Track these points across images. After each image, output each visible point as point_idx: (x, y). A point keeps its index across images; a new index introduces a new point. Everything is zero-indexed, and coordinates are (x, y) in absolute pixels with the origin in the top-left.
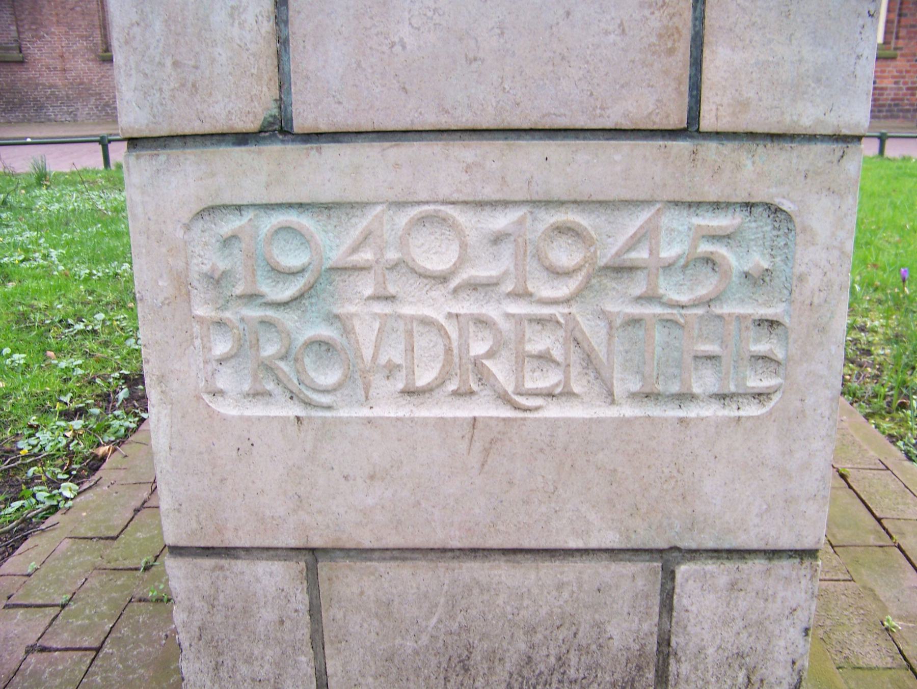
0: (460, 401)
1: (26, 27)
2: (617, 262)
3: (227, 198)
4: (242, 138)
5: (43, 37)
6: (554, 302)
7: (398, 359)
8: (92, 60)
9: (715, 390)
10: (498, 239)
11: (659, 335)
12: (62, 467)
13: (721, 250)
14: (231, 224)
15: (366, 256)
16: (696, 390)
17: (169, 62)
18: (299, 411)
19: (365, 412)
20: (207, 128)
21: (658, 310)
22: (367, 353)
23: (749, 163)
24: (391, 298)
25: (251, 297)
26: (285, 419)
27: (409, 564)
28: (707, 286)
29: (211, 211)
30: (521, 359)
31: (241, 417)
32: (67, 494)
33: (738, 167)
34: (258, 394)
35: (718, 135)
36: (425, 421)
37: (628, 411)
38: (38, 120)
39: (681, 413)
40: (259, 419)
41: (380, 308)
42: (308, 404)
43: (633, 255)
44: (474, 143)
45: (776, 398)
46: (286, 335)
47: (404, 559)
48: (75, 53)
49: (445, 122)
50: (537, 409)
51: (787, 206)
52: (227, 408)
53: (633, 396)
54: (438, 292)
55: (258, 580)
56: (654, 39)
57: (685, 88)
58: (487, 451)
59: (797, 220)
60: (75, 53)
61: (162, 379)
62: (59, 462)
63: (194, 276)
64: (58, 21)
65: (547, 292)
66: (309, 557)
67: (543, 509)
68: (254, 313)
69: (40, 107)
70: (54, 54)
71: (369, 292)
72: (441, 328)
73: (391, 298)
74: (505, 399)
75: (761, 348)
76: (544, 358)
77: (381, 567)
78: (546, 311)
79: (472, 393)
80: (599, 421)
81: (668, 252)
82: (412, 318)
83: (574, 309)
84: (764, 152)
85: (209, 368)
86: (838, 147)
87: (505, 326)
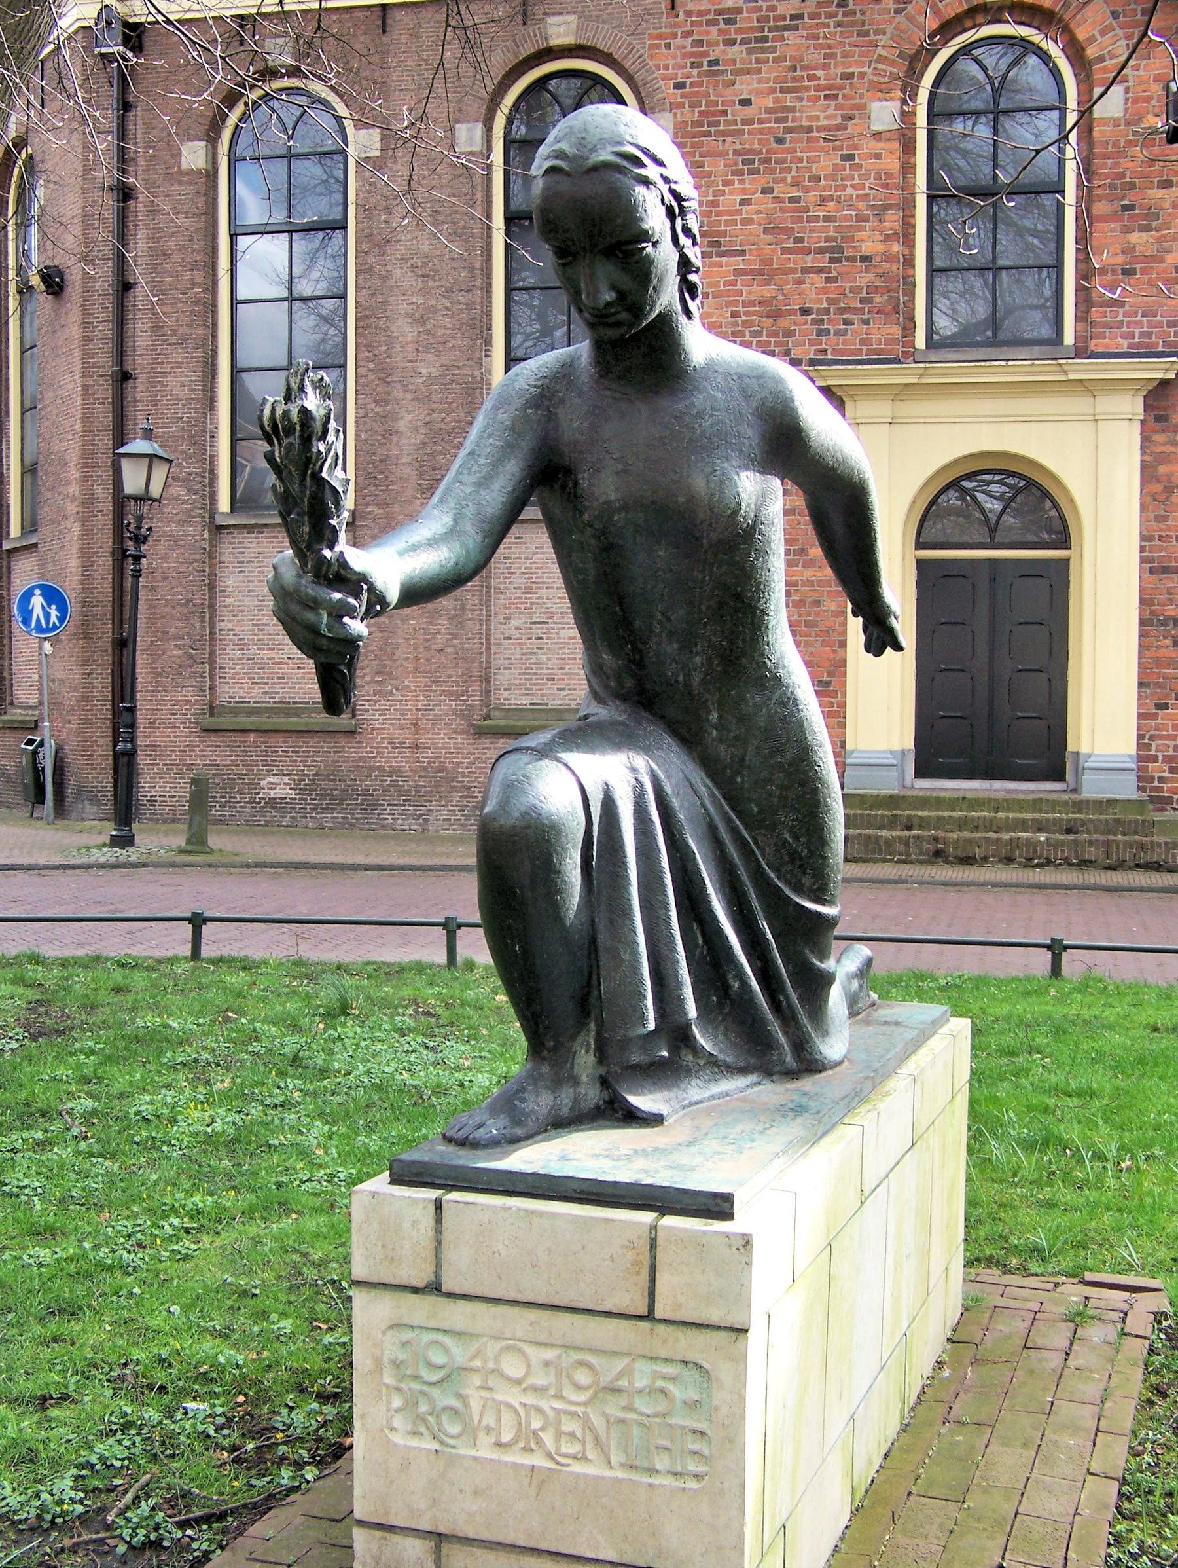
0: (526, 1454)
1: (368, 678)
2: (611, 1386)
3: (405, 1321)
4: (416, 1290)
5: (391, 693)
6: (577, 1404)
7: (493, 1424)
8: (463, 732)
9: (669, 1468)
10: (547, 1364)
11: (636, 1431)
12: (309, 1451)
13: (670, 1387)
14: (408, 1335)
15: (477, 1363)
16: (658, 1467)
17: (380, 1244)
18: (437, 1446)
19: (473, 1453)
20: (397, 1282)
21: (635, 1416)
22: (476, 1419)
23: (682, 1338)
24: (490, 1389)
25: (416, 1377)
26: (428, 1450)
27: (494, 1553)
28: (662, 1406)
29: (397, 1326)
30: (559, 1434)
31: (405, 1446)
32: (309, 1477)
33: (677, 1340)
34: (415, 1433)
35: (665, 1321)
36: (506, 1463)
37: (620, 1474)
38: (367, 826)
39: (650, 1480)
40: (415, 1448)
41: (484, 1393)
42: (442, 1443)
43: (620, 1383)
44: (536, 1311)
45: (706, 1478)
46: (432, 1401)
47: (492, 1549)
48: (435, 721)
49: (520, 1297)
50: (569, 1465)
51: (705, 1365)
52: (398, 1439)
53: (622, 1465)
54: (516, 1390)
55: (406, 1550)
56: (629, 1266)
57: (646, 1293)
58: (540, 1487)
59: (712, 1374)
60: (435, 721)
61: (363, 1416)
62: (307, 1445)
63: (385, 1360)
64: (416, 669)
65: (574, 1397)
66: (437, 1538)
67: (572, 1528)
68: (416, 1386)
69: (371, 805)
70: (403, 721)
71: (478, 1384)
72: (516, 1411)
73: (490, 1389)
74: (550, 1456)
75: (696, 1447)
76: (572, 1435)
77: (478, 1552)
78: (573, 1408)
79: (532, 1450)
80: (603, 1478)
81: (640, 1383)
82: (501, 1402)
83: (589, 1410)
84: (691, 1333)
85: (389, 1415)
86: (733, 1335)
87: (550, 1413)
